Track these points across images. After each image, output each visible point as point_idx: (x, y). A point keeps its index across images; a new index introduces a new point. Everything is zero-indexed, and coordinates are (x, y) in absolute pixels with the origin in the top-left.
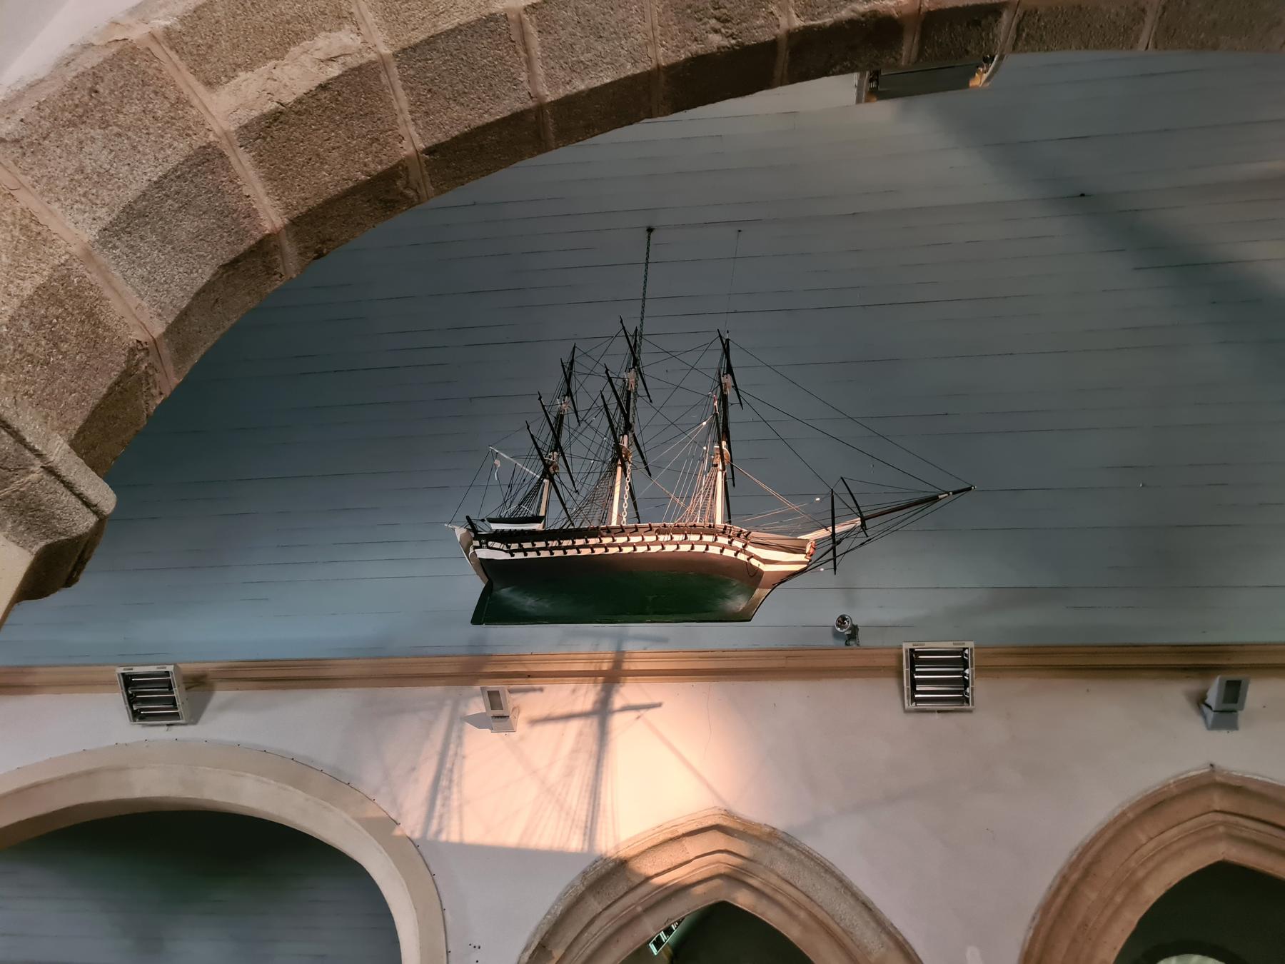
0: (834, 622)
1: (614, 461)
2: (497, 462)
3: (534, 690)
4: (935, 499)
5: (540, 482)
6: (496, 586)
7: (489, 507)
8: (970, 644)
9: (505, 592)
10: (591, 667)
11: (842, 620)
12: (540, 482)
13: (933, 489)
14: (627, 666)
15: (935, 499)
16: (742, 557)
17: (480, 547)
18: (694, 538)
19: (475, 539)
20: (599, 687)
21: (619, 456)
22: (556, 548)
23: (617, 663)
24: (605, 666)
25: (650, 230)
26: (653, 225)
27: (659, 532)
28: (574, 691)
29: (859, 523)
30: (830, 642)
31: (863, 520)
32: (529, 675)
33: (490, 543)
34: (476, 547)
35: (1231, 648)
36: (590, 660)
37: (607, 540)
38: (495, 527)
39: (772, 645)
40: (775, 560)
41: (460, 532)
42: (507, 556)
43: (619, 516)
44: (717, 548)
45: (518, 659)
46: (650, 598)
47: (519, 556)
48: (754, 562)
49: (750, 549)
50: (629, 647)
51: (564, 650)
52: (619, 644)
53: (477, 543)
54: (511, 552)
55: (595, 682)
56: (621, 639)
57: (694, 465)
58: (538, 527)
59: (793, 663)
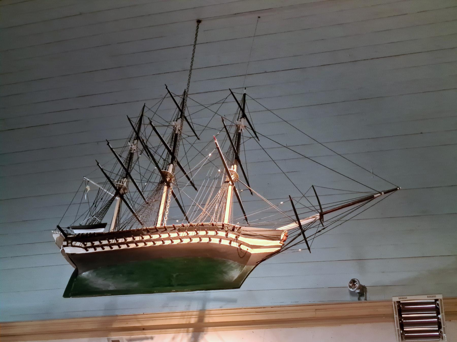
0: (347, 284)
1: (162, 183)
2: (88, 187)
3: (147, 338)
4: (371, 198)
5: (113, 199)
6: (80, 271)
7: (77, 218)
8: (439, 297)
9: (85, 274)
10: (183, 321)
11: (353, 282)
12: (113, 199)
13: (371, 190)
14: (207, 320)
15: (371, 198)
16: (235, 244)
17: (67, 246)
18: (202, 233)
19: (64, 241)
20: (190, 335)
21: (164, 180)
22: (114, 244)
23: (201, 318)
24: (193, 320)
25: (199, 22)
26: (200, 18)
27: (180, 230)
28: (173, 338)
29: (318, 217)
30: (348, 298)
31: (322, 215)
32: (144, 329)
33: (74, 243)
34: (64, 246)
35: (17, 324)
36: (183, 316)
37: (146, 237)
38: (77, 232)
39: (306, 301)
40: (257, 245)
41: (57, 235)
42: (83, 251)
43: (163, 220)
44: (219, 240)
45: (135, 317)
46: (175, 275)
47: (91, 250)
48: (244, 248)
49: (241, 239)
50: (210, 306)
51: (166, 310)
52: (204, 305)
53: (65, 243)
54: (86, 248)
55: (188, 332)
56: (205, 301)
57: (210, 183)
58: (101, 230)
59: (320, 314)
